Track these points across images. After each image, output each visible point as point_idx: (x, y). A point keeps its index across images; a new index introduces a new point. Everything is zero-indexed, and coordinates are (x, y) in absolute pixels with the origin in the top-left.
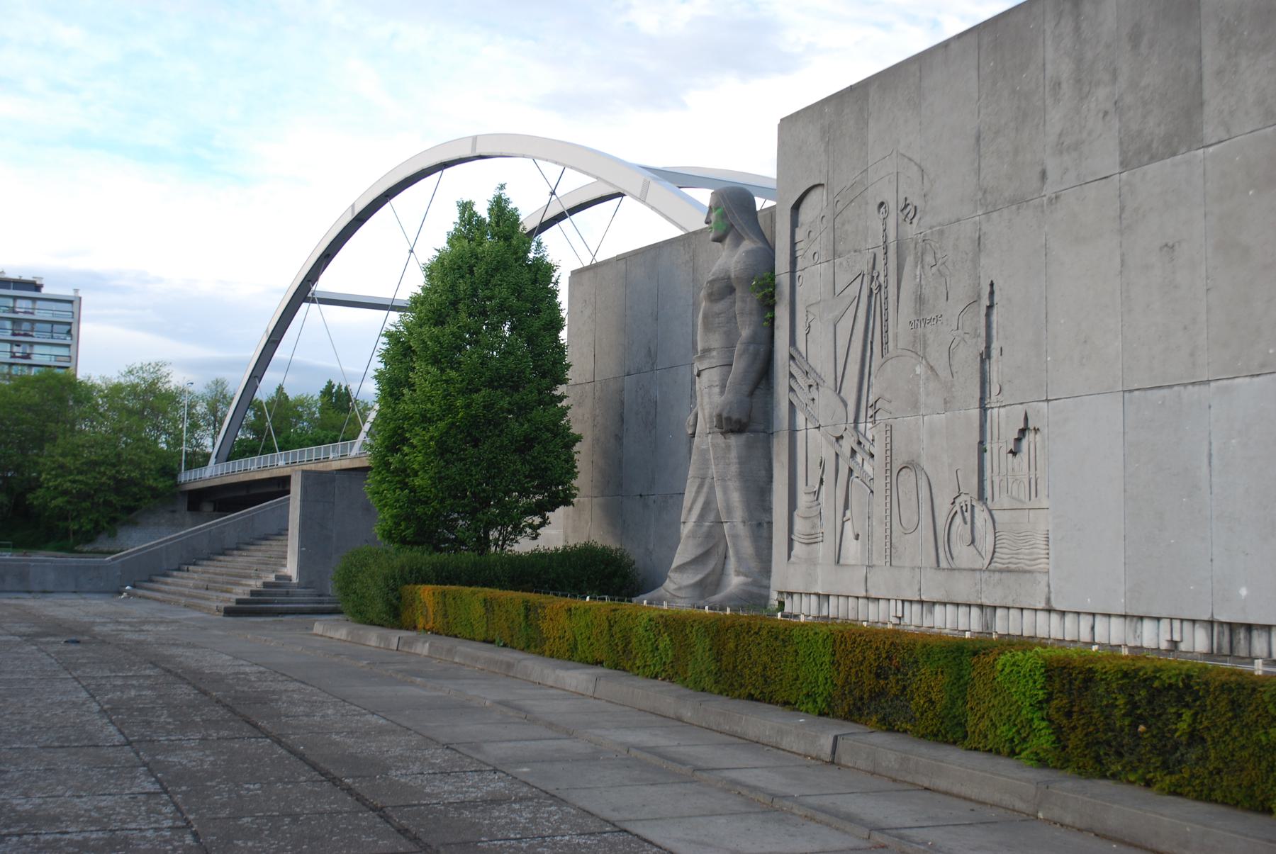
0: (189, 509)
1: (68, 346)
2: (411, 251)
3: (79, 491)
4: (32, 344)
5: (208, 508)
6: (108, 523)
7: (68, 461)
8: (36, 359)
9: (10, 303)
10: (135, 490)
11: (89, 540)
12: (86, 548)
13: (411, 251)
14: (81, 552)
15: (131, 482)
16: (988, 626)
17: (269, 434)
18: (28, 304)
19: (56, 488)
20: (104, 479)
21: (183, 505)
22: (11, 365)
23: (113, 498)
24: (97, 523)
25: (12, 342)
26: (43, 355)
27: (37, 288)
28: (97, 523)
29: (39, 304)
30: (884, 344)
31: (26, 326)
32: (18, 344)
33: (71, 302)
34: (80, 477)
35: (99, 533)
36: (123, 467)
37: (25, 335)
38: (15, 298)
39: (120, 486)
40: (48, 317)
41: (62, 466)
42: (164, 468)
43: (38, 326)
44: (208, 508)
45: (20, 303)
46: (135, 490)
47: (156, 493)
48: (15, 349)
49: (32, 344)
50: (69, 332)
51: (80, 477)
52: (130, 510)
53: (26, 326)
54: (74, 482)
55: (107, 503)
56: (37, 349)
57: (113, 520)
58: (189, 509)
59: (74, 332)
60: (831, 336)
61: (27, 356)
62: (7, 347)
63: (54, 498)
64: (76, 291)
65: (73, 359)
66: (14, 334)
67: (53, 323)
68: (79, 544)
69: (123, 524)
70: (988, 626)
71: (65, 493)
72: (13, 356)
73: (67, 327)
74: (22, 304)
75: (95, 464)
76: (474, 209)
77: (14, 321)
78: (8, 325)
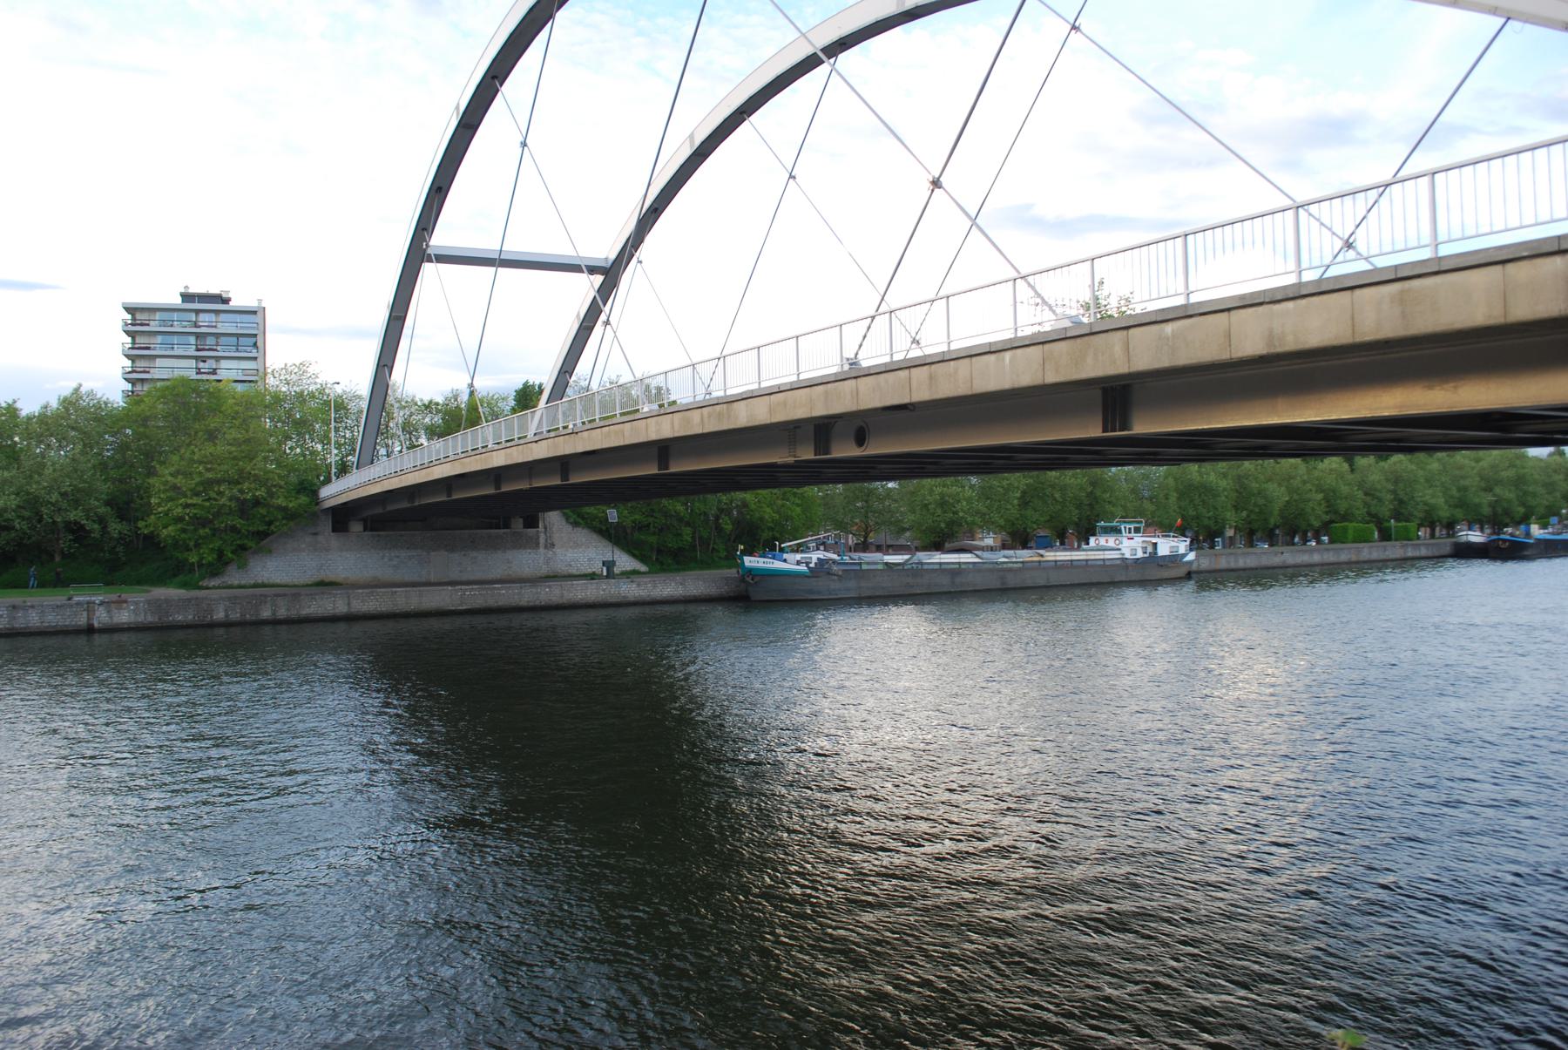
2: (524, 144)
3: (195, 517)
4: (218, 359)
5: (356, 527)
6: (233, 552)
7: (179, 480)
9: (193, 317)
10: (263, 511)
11: (215, 574)
13: (524, 144)
14: (207, 588)
15: (257, 502)
16: (1096, 285)
18: (213, 317)
20: (223, 501)
21: (326, 525)
23: (238, 522)
24: (221, 554)
25: (196, 358)
27: (226, 301)
28: (221, 554)
29: (223, 317)
33: (255, 313)
34: (195, 500)
35: (227, 564)
36: (246, 485)
38: (198, 312)
39: (245, 508)
41: (175, 488)
42: (301, 483)
43: (223, 340)
44: (356, 527)
45: (202, 317)
46: (263, 511)
47: (290, 515)
48: (201, 365)
49: (218, 359)
50: (255, 345)
51: (195, 500)
52: (262, 535)
53: (210, 341)
54: (187, 506)
55: (233, 529)
56: (224, 364)
57: (243, 548)
59: (260, 344)
61: (214, 372)
62: (193, 363)
63: (165, 527)
67: (238, 336)
68: (203, 578)
69: (255, 553)
70: (1096, 285)
71: (180, 519)
73: (251, 341)
75: (209, 484)
77: (198, 336)
78: (192, 340)
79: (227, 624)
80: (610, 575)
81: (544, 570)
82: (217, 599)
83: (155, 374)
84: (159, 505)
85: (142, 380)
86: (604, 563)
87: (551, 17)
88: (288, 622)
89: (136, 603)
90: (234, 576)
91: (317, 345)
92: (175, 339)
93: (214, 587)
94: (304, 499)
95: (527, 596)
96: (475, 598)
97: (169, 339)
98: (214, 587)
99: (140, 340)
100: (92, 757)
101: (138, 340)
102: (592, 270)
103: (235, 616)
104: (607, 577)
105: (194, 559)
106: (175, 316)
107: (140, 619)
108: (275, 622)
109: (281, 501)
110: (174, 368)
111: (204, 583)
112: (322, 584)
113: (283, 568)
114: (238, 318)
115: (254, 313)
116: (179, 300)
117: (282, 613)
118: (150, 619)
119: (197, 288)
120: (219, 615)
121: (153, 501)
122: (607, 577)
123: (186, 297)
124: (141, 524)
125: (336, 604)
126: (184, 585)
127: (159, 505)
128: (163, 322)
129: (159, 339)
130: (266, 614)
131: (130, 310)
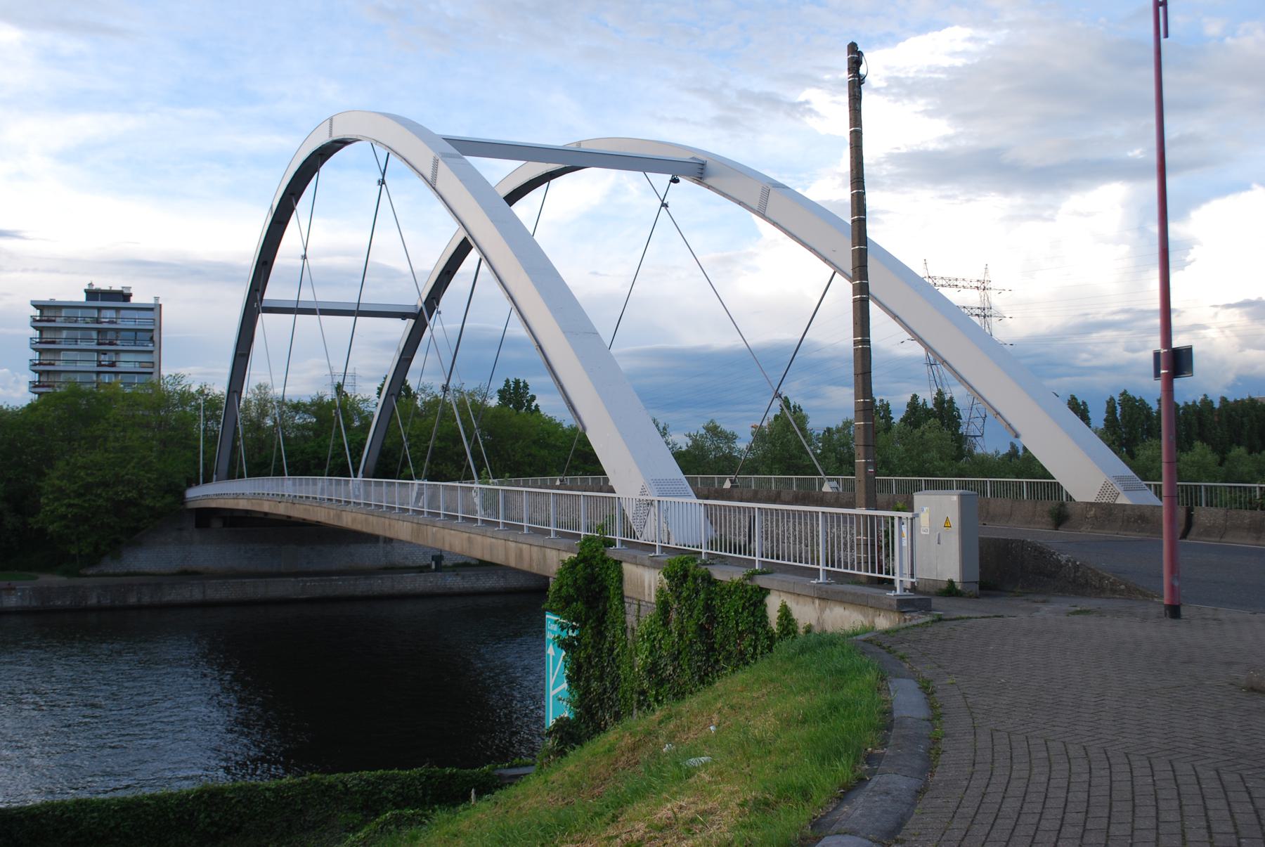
0: (197, 526)
1: (151, 352)
4: (117, 352)
5: (217, 524)
7: (64, 483)
8: (122, 367)
12: (90, 572)
14: (86, 576)
17: (338, 426)
19: (52, 512)
20: (100, 502)
22: (98, 373)
25: (98, 351)
26: (127, 362)
29: (123, 313)
30: (54, 343)
31: (110, 336)
32: (105, 352)
33: (152, 309)
37: (111, 344)
38: (100, 309)
40: (131, 325)
41: (60, 490)
48: (102, 357)
49: (117, 352)
50: (152, 339)
51: (76, 501)
53: (110, 336)
54: (70, 505)
56: (123, 357)
58: (197, 526)
59: (156, 338)
60: (440, 206)
61: (113, 364)
63: (52, 522)
64: (157, 299)
65: (155, 365)
66: (99, 344)
67: (136, 331)
71: (64, 517)
72: (100, 365)
73: (150, 334)
74: (109, 314)
76: (1013, 325)
77: (99, 331)
78: (94, 334)
79: (99, 609)
80: (439, 568)
81: (383, 562)
82: (92, 587)
83: (60, 366)
84: (47, 505)
85: (48, 372)
86: (433, 558)
87: (293, 209)
88: (150, 607)
89: (23, 590)
90: (109, 566)
91: (193, 359)
92: (79, 334)
93: (92, 575)
94: (169, 499)
95: (362, 586)
96: (315, 587)
97: (73, 334)
98: (92, 575)
99: (47, 335)
100: (102, 747)
101: (45, 336)
102: (403, 316)
103: (106, 602)
104: (437, 570)
105: (74, 551)
106: (79, 313)
107: (26, 603)
108: (139, 608)
109: (148, 502)
110: (79, 364)
111: (82, 572)
112: (184, 573)
113: (150, 559)
114: (136, 314)
115: (154, 309)
116: (82, 298)
117: (146, 600)
118: (34, 604)
119: (103, 284)
120: (93, 601)
121: (43, 500)
122: (437, 570)
123: (92, 294)
124: (31, 520)
125: (192, 593)
126: (66, 573)
127: (47, 505)
128: (68, 319)
129: (64, 334)
130: (132, 600)
131: (37, 306)
